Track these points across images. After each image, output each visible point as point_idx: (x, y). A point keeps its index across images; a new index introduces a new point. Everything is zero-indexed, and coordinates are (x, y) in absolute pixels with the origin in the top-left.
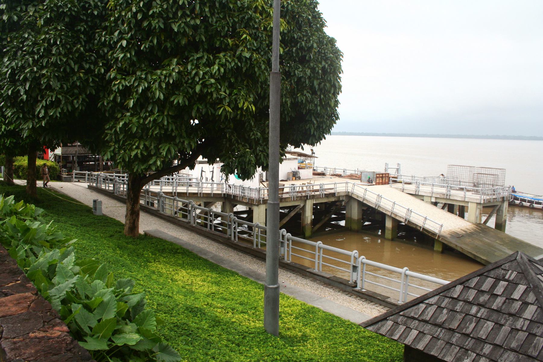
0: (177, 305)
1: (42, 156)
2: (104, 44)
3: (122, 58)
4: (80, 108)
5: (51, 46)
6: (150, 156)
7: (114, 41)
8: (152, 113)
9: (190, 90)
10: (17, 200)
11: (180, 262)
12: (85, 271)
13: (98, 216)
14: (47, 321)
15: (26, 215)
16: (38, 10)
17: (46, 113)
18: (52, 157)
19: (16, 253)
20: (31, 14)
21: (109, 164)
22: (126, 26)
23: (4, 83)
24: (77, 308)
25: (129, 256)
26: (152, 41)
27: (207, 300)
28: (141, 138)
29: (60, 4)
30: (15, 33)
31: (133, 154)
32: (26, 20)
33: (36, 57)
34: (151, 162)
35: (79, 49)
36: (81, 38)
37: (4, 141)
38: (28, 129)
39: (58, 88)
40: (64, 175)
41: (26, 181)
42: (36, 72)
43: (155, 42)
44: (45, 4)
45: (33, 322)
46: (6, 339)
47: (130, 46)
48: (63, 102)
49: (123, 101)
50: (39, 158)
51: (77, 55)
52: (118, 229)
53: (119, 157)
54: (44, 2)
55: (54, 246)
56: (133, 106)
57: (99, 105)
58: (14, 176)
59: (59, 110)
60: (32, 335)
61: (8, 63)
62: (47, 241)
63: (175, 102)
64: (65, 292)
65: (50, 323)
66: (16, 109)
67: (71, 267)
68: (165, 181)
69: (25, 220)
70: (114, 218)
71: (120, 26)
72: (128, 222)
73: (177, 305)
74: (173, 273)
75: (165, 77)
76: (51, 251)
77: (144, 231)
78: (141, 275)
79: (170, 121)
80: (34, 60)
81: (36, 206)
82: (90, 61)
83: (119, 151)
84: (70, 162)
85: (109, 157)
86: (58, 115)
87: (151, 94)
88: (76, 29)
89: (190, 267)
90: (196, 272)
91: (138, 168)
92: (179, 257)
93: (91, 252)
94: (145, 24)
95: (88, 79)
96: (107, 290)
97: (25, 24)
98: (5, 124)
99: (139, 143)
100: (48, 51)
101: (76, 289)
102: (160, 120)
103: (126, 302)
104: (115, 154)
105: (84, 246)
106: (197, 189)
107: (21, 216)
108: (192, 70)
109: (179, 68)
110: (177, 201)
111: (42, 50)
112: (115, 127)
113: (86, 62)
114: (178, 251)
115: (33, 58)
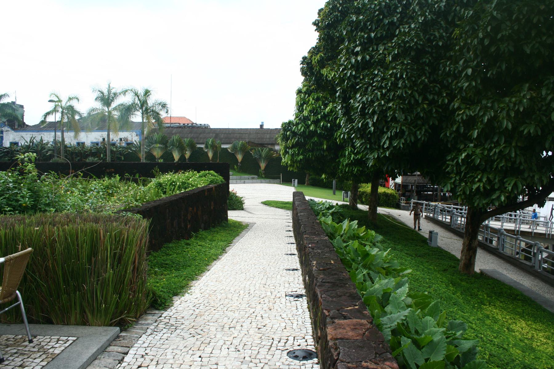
0: (513, 361)
1: (384, 183)
2: (448, 74)
3: (467, 87)
4: (423, 139)
5: (397, 79)
6: (493, 190)
7: (459, 70)
8: (497, 144)
9: (544, 118)
10: (360, 225)
11: (520, 310)
12: (417, 305)
13: (432, 248)
14: (379, 353)
15: (366, 240)
16: (387, 48)
17: (390, 144)
18: (393, 185)
19: (355, 275)
20: (381, 52)
21: (447, 194)
22: (472, 54)
23: (356, 116)
24: (406, 342)
25: (462, 294)
26: (500, 67)
27: (552, 362)
28: (484, 171)
29: (407, 39)
30: (366, 71)
31: (475, 187)
32: (377, 58)
33: (384, 91)
34: (494, 197)
35: (424, 81)
36: (426, 69)
37: (352, 169)
38: (374, 158)
39: (402, 120)
40: (403, 203)
41: (368, 207)
42: (384, 105)
43: (504, 67)
44: (393, 41)
45: (366, 351)
46: (342, 361)
47: (476, 74)
48: (407, 133)
49: (467, 131)
50: (381, 185)
51: (421, 87)
52: (452, 264)
53: (460, 189)
54: (393, 40)
55: (389, 274)
56: (477, 136)
57: (442, 135)
58: (358, 201)
59: (403, 141)
60: (364, 364)
61: (360, 98)
62: (383, 268)
63: (525, 132)
64: (396, 324)
65: (382, 356)
66: (365, 140)
67: (403, 298)
68: (506, 217)
69: (365, 245)
70: (449, 251)
71: (466, 54)
72: (464, 258)
73: (513, 361)
74: (510, 321)
75: (515, 104)
76: (386, 278)
77: (480, 270)
78: (473, 318)
79: (518, 152)
80: (382, 94)
81: (376, 232)
82: (434, 92)
83: (460, 183)
84: (409, 191)
85: (449, 189)
86: (402, 146)
87: (498, 123)
88: (421, 61)
89: (532, 319)
90: (538, 326)
91: (478, 202)
92: (519, 304)
93: (424, 284)
94: (493, 49)
95: (431, 110)
96: (438, 329)
97: (375, 62)
98: (354, 153)
99: (482, 175)
100: (395, 85)
101: (407, 322)
102: (507, 152)
103: (456, 346)
104: (455, 186)
105: (417, 278)
106: (544, 229)
107: (362, 240)
108: (547, 95)
109: (531, 94)
110: (521, 240)
111: (390, 85)
112: (457, 158)
113: (431, 93)
114: (518, 298)
115: (381, 92)
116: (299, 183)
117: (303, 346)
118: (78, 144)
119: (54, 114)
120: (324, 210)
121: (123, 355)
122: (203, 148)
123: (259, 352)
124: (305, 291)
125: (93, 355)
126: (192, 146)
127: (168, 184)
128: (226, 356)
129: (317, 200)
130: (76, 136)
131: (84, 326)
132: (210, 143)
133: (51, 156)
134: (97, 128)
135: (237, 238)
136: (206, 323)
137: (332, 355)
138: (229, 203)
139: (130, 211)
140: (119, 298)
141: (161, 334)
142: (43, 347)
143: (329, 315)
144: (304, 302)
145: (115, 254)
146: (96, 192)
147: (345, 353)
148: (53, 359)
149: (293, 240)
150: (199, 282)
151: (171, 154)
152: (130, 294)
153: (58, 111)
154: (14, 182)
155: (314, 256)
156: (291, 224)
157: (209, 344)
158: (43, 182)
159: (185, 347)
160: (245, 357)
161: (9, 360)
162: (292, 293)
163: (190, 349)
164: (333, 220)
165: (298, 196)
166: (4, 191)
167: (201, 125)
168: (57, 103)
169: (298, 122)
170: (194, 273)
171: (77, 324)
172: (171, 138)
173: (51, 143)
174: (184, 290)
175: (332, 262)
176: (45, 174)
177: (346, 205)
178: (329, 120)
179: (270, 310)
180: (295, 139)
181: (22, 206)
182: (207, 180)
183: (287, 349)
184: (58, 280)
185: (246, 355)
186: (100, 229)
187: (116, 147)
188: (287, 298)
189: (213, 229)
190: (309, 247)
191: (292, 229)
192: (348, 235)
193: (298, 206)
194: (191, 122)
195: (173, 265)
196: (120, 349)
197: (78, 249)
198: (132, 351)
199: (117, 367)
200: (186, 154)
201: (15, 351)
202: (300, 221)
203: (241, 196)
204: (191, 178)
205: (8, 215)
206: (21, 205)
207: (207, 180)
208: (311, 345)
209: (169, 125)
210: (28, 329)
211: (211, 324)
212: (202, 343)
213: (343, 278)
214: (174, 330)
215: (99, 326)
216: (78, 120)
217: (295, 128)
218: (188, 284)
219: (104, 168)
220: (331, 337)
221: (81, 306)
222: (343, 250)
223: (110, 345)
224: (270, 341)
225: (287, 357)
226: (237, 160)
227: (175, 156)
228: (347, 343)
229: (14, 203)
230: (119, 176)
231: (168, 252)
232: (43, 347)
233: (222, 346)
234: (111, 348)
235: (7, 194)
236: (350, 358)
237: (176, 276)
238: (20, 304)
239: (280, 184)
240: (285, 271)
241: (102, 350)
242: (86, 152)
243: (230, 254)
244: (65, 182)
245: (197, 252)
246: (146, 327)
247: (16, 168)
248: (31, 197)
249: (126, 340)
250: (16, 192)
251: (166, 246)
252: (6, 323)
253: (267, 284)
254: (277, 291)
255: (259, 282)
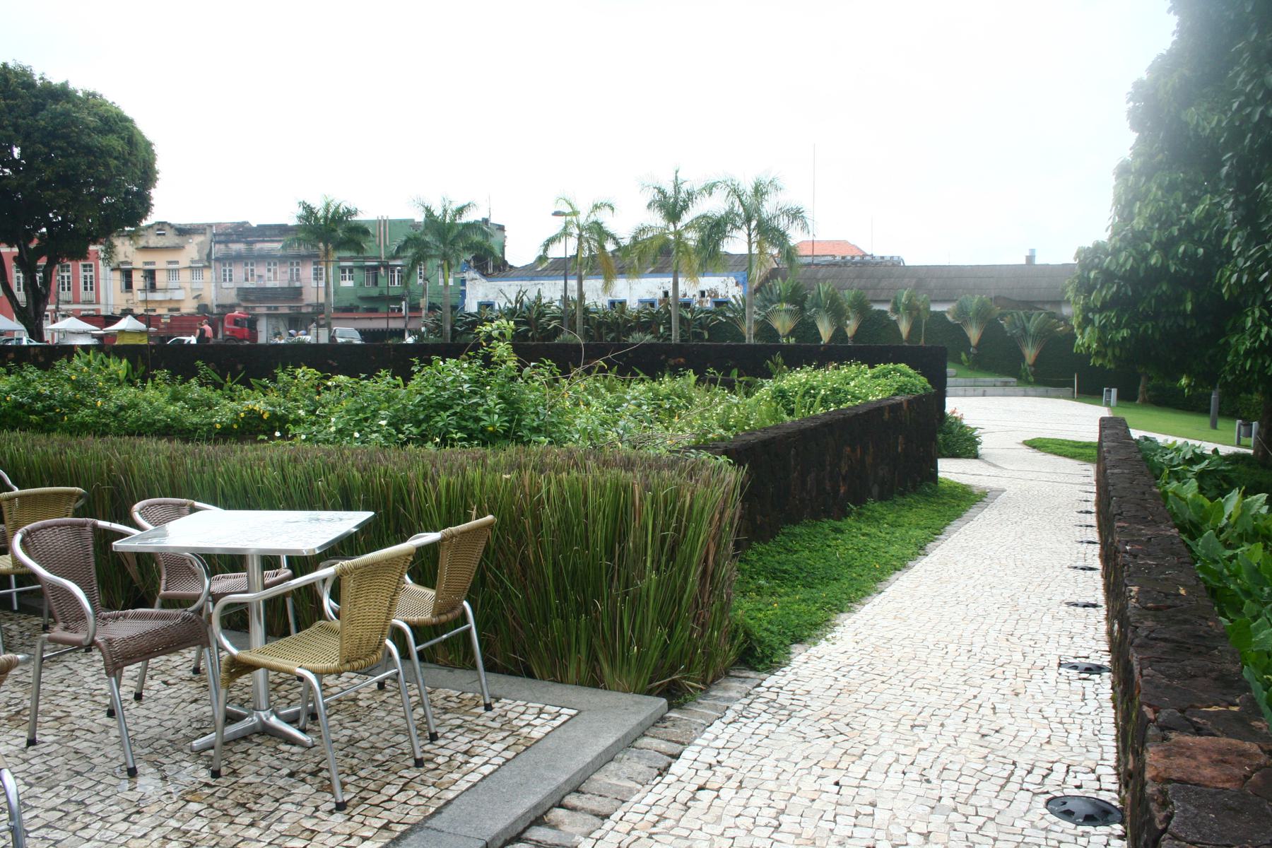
37: (1264, 363)
45: (1248, 823)
46: (1175, 837)
116: (1120, 397)
117: (1090, 789)
118: (612, 303)
119: (563, 240)
120: (1179, 465)
121: (669, 759)
122: (886, 312)
123: (976, 790)
124: (1109, 658)
125: (607, 750)
126: (861, 306)
127: (800, 393)
128: (898, 788)
129: (1161, 439)
130: (606, 289)
131: (595, 690)
132: (903, 300)
133: (557, 331)
134: (651, 269)
135: (956, 523)
136: (859, 709)
137: (1152, 819)
138: (944, 441)
139: (707, 448)
140: (670, 636)
141: (756, 724)
142: (510, 721)
143: (1156, 719)
144: (1104, 685)
145: (664, 539)
146: (635, 405)
147: (1186, 818)
148: (527, 748)
149: (1094, 535)
150: (854, 616)
151: (814, 326)
152: (693, 630)
153: (571, 235)
154: (474, 381)
155: (1135, 572)
156: (1093, 497)
157: (860, 758)
158: (530, 381)
159: (807, 757)
160: (941, 798)
161: (446, 738)
162: (1076, 661)
163: (816, 764)
164: (1201, 489)
165: (1111, 428)
166: (454, 399)
167: (882, 258)
168: (569, 218)
169: (1118, 245)
170: (845, 597)
171: (580, 683)
172: (813, 289)
173: (557, 303)
174: (819, 633)
175: (1182, 592)
176: (532, 364)
177: (1244, 457)
178: (1200, 239)
179: (1017, 695)
180: (1109, 288)
181: (486, 431)
182: (891, 386)
183: (1047, 793)
184: (545, 586)
185: (944, 794)
186: (633, 484)
187: (693, 311)
188: (1062, 670)
189: (900, 500)
190: (1126, 552)
191: (1094, 509)
192: (1239, 530)
193: (1109, 452)
194: (861, 251)
195: (800, 576)
196: (664, 746)
197: (586, 525)
198: (689, 754)
199: (655, 783)
200: (847, 326)
201: (459, 722)
202: (1110, 488)
203: (973, 426)
204: (853, 379)
205: (457, 449)
206: (483, 429)
207: (891, 386)
208: (1109, 790)
209: (809, 260)
210: (484, 681)
211: (871, 713)
212: (845, 753)
213: (1205, 632)
214: (785, 718)
215: (625, 691)
216: (613, 252)
217: (1111, 261)
218: (828, 620)
219: (663, 357)
220: (1154, 773)
221: (590, 646)
222: (1221, 565)
223: (644, 735)
224: (1006, 767)
225: (1046, 811)
226: (967, 340)
227: (822, 331)
228: (1196, 793)
229: (470, 424)
230: (695, 374)
231: (790, 544)
232: (510, 721)
233: (890, 765)
234: (645, 742)
235: (458, 405)
236: (1199, 832)
237: (804, 600)
238: (469, 630)
239: (1072, 398)
240: (1064, 607)
241: (626, 743)
242: (629, 321)
243: (934, 559)
244: (580, 384)
245: (858, 550)
246: (726, 704)
247: (477, 353)
248: (504, 412)
249: (680, 728)
250: (476, 403)
251: (786, 531)
252: (446, 665)
253: (1017, 633)
254: (1038, 653)
255: (998, 627)
